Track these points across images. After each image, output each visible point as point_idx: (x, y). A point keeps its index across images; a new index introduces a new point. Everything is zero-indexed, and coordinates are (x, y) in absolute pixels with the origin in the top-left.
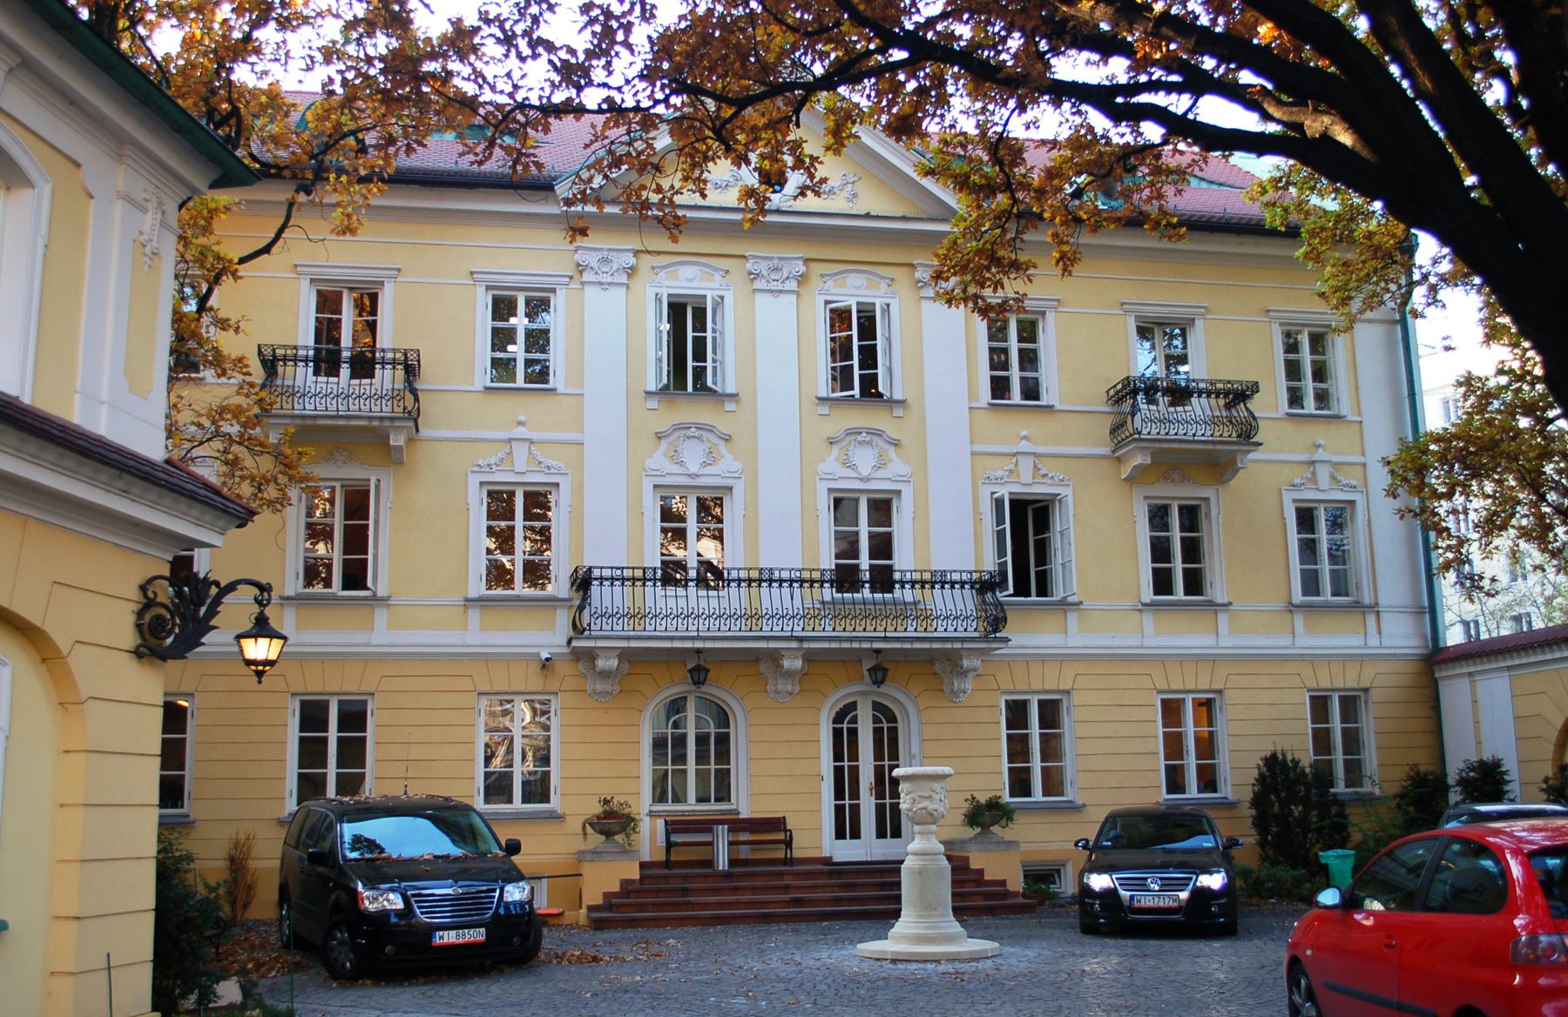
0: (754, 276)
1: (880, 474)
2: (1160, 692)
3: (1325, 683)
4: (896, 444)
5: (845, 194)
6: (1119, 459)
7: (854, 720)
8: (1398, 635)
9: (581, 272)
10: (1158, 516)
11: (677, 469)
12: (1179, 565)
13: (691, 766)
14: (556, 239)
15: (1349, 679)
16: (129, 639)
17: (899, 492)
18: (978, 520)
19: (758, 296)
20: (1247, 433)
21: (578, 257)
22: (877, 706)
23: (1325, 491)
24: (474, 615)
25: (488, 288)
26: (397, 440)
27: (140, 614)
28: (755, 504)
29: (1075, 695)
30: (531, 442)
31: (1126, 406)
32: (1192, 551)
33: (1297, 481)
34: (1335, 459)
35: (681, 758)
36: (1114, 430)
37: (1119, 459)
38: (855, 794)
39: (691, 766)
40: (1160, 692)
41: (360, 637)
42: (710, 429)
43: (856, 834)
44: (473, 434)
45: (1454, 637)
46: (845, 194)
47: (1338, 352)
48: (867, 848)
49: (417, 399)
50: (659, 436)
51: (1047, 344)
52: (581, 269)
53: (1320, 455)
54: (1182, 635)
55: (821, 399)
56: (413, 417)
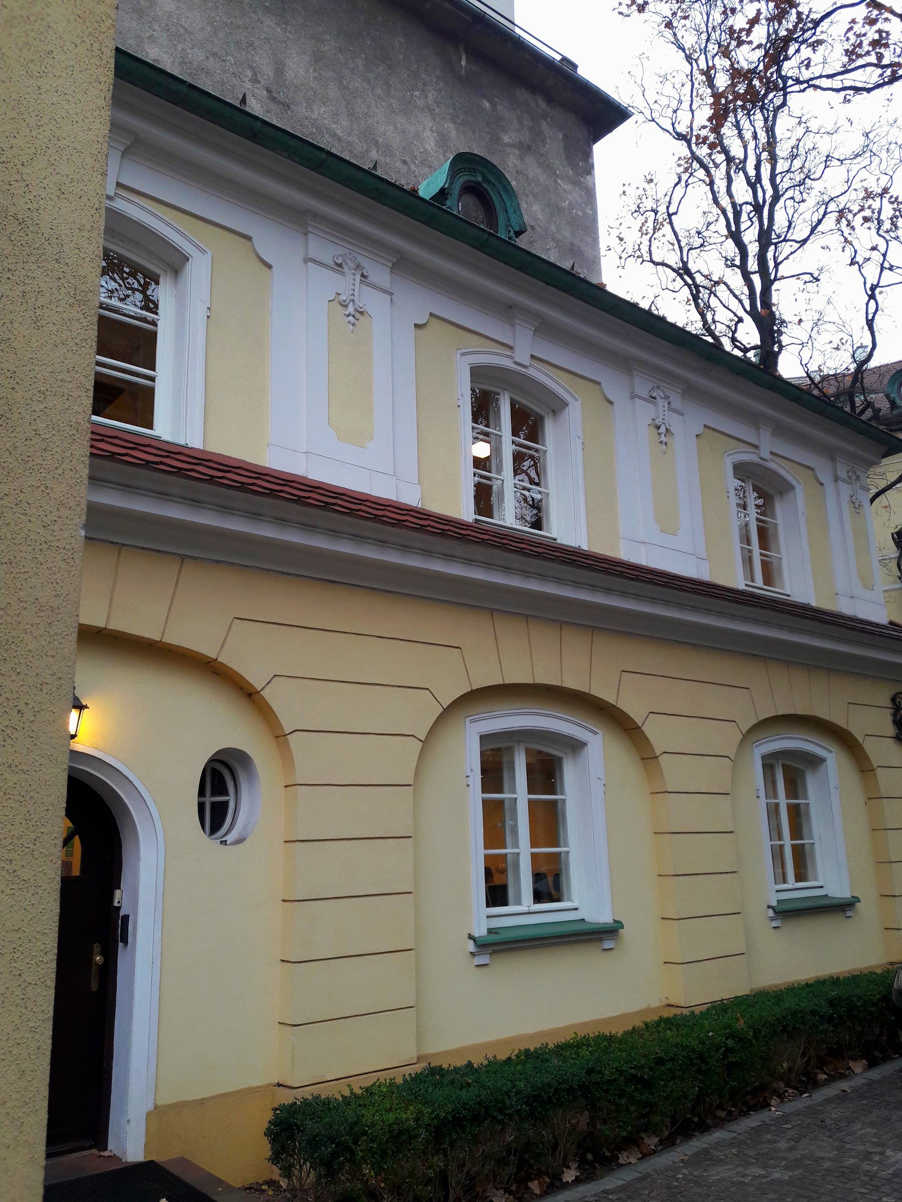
27: (894, 715)
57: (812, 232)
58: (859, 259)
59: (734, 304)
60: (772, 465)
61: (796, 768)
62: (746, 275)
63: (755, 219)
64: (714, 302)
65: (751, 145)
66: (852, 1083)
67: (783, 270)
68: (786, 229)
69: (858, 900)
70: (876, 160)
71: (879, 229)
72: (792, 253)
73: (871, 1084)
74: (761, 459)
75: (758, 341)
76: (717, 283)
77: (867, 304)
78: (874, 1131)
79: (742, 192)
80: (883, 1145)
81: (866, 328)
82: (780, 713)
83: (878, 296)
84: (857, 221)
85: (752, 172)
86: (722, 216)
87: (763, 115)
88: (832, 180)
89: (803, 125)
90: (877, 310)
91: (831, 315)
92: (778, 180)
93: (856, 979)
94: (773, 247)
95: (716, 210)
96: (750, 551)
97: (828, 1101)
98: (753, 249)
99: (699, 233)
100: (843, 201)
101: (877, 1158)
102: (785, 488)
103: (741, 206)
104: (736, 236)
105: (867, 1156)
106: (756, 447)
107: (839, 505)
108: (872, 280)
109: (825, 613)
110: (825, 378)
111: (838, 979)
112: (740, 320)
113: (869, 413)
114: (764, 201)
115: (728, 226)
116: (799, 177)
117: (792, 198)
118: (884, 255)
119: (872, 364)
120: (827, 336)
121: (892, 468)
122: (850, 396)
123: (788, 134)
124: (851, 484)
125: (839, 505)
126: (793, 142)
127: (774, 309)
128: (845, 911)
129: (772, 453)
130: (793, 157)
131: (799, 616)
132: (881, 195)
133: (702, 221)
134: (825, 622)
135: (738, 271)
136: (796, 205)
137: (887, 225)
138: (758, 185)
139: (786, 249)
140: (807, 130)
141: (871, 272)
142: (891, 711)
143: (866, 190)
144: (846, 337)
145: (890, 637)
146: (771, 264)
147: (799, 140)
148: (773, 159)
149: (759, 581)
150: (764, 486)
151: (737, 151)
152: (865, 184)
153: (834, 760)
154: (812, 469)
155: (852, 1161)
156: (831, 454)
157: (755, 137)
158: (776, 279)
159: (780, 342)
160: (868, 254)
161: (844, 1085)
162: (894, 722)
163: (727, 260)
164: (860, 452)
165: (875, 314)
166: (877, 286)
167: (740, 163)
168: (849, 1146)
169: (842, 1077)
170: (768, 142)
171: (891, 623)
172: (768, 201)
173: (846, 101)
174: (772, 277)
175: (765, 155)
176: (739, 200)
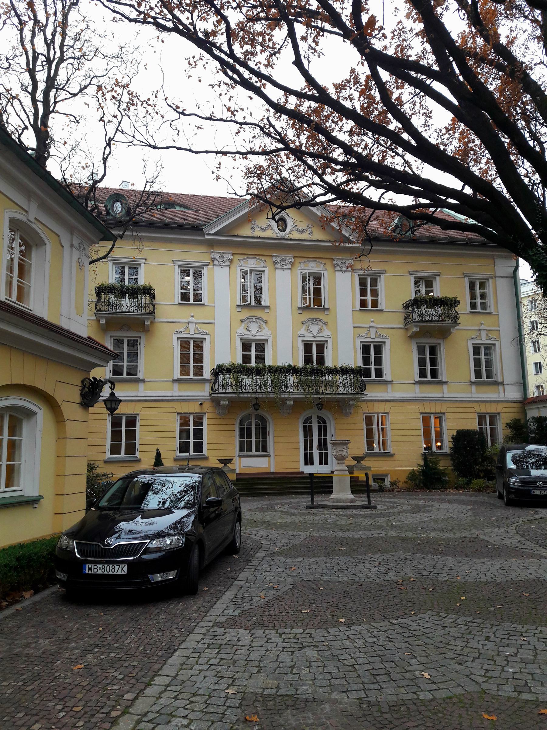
0: (275, 263)
1: (320, 335)
2: (421, 413)
3: (483, 411)
4: (326, 324)
5: (308, 232)
6: (407, 329)
7: (311, 422)
8: (512, 393)
9: (213, 261)
10: (421, 350)
11: (248, 333)
12: (429, 369)
13: (253, 439)
14: (203, 250)
15: (492, 409)
16: (78, 399)
17: (327, 341)
18: (355, 351)
19: (277, 270)
20: (455, 319)
21: (212, 256)
22: (319, 417)
23: (484, 340)
24: (176, 385)
25: (179, 267)
26: (147, 323)
27: (82, 391)
28: (276, 346)
29: (447, 414)
30: (196, 323)
31: (410, 310)
32: (434, 362)
33: (474, 337)
34: (488, 328)
35: (249, 436)
36: (405, 319)
37: (407, 329)
38: (311, 449)
39: (253, 439)
40: (421, 413)
41: (134, 394)
42: (260, 319)
43: (312, 464)
44: (173, 318)
45: (532, 393)
46: (308, 232)
47: (490, 290)
48: (316, 469)
49: (154, 308)
50: (242, 321)
51: (381, 287)
52: (213, 260)
53: (482, 327)
54: (431, 393)
55: (299, 308)
56: (152, 313)
57: (81, 91)
58: (105, 119)
59: (23, 116)
60: (34, 226)
61: (15, 416)
62: (34, 101)
63: (45, 67)
64: (9, 109)
65: (52, 19)
66: (23, 605)
67: (59, 107)
68: (65, 82)
69: (41, 497)
70: (124, 66)
71: (119, 107)
72: (66, 99)
73: (35, 604)
74: (28, 220)
75: (35, 147)
76: (14, 98)
77: (105, 148)
78: (33, 630)
79: (40, 47)
80: (38, 637)
81: (102, 162)
82: (14, 382)
83: (112, 146)
84: (109, 96)
85: (49, 37)
86: (24, 56)
87: (63, 4)
88: (97, 65)
89: (85, 23)
90: (110, 154)
91: (83, 146)
92: (65, 48)
93: (34, 543)
94: (54, 90)
95: (21, 50)
96: (11, 277)
97: (7, 617)
98: (42, 86)
99: (7, 59)
100: (102, 80)
101: (33, 645)
102: (40, 243)
103: (38, 54)
104: (32, 73)
105: (28, 645)
106: (26, 212)
107: (71, 263)
108: (110, 135)
109: (52, 324)
110: (72, 184)
111: (23, 544)
112: (26, 128)
113: (95, 213)
114: (54, 59)
115: (28, 63)
116: (77, 54)
117: (72, 64)
118: (120, 123)
119: (100, 185)
120: (78, 158)
121: (102, 249)
122: (87, 199)
123: (75, 24)
124: (80, 251)
125: (71, 263)
126: (78, 30)
127: (49, 129)
128: (33, 504)
129: (35, 218)
130: (77, 39)
131: (37, 324)
132: (124, 87)
133: (11, 52)
134: (52, 330)
135: (30, 96)
136: (74, 70)
137: (124, 106)
138: (52, 47)
139: (63, 95)
140: (88, 27)
141: (111, 129)
142: (80, 388)
143: (116, 80)
144: (90, 163)
145: (88, 345)
146: (52, 100)
147: (82, 31)
148: (64, 35)
149: (14, 298)
150: (27, 240)
151: (41, 17)
152: (116, 77)
153: (42, 414)
154: (59, 236)
155: (18, 650)
156: (71, 230)
157: (55, 14)
158: (53, 111)
159: (49, 152)
160: (111, 118)
161: (18, 607)
162: (81, 394)
163: (22, 85)
164: (88, 234)
165: (108, 155)
166: (112, 139)
167: (43, 26)
168: (18, 641)
169: (17, 602)
170: (63, 23)
171: (89, 337)
172: (57, 60)
173: (114, 20)
174: (51, 109)
175: (59, 29)
176: (38, 50)
